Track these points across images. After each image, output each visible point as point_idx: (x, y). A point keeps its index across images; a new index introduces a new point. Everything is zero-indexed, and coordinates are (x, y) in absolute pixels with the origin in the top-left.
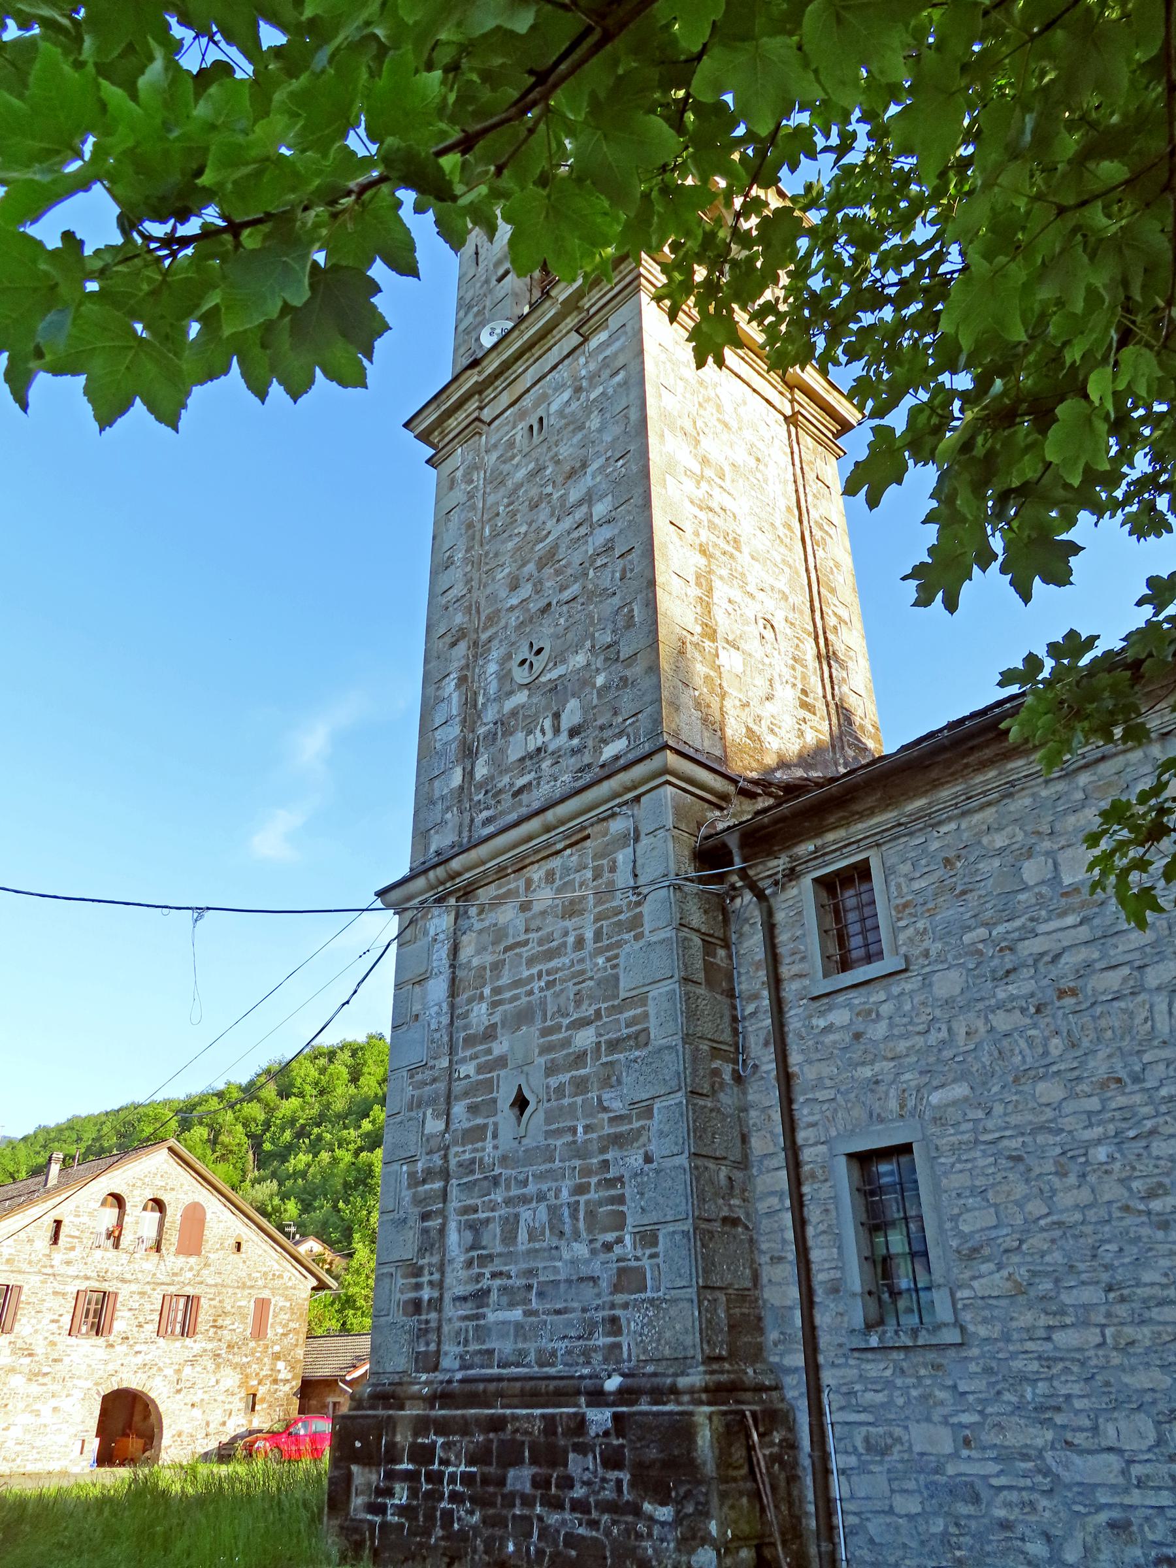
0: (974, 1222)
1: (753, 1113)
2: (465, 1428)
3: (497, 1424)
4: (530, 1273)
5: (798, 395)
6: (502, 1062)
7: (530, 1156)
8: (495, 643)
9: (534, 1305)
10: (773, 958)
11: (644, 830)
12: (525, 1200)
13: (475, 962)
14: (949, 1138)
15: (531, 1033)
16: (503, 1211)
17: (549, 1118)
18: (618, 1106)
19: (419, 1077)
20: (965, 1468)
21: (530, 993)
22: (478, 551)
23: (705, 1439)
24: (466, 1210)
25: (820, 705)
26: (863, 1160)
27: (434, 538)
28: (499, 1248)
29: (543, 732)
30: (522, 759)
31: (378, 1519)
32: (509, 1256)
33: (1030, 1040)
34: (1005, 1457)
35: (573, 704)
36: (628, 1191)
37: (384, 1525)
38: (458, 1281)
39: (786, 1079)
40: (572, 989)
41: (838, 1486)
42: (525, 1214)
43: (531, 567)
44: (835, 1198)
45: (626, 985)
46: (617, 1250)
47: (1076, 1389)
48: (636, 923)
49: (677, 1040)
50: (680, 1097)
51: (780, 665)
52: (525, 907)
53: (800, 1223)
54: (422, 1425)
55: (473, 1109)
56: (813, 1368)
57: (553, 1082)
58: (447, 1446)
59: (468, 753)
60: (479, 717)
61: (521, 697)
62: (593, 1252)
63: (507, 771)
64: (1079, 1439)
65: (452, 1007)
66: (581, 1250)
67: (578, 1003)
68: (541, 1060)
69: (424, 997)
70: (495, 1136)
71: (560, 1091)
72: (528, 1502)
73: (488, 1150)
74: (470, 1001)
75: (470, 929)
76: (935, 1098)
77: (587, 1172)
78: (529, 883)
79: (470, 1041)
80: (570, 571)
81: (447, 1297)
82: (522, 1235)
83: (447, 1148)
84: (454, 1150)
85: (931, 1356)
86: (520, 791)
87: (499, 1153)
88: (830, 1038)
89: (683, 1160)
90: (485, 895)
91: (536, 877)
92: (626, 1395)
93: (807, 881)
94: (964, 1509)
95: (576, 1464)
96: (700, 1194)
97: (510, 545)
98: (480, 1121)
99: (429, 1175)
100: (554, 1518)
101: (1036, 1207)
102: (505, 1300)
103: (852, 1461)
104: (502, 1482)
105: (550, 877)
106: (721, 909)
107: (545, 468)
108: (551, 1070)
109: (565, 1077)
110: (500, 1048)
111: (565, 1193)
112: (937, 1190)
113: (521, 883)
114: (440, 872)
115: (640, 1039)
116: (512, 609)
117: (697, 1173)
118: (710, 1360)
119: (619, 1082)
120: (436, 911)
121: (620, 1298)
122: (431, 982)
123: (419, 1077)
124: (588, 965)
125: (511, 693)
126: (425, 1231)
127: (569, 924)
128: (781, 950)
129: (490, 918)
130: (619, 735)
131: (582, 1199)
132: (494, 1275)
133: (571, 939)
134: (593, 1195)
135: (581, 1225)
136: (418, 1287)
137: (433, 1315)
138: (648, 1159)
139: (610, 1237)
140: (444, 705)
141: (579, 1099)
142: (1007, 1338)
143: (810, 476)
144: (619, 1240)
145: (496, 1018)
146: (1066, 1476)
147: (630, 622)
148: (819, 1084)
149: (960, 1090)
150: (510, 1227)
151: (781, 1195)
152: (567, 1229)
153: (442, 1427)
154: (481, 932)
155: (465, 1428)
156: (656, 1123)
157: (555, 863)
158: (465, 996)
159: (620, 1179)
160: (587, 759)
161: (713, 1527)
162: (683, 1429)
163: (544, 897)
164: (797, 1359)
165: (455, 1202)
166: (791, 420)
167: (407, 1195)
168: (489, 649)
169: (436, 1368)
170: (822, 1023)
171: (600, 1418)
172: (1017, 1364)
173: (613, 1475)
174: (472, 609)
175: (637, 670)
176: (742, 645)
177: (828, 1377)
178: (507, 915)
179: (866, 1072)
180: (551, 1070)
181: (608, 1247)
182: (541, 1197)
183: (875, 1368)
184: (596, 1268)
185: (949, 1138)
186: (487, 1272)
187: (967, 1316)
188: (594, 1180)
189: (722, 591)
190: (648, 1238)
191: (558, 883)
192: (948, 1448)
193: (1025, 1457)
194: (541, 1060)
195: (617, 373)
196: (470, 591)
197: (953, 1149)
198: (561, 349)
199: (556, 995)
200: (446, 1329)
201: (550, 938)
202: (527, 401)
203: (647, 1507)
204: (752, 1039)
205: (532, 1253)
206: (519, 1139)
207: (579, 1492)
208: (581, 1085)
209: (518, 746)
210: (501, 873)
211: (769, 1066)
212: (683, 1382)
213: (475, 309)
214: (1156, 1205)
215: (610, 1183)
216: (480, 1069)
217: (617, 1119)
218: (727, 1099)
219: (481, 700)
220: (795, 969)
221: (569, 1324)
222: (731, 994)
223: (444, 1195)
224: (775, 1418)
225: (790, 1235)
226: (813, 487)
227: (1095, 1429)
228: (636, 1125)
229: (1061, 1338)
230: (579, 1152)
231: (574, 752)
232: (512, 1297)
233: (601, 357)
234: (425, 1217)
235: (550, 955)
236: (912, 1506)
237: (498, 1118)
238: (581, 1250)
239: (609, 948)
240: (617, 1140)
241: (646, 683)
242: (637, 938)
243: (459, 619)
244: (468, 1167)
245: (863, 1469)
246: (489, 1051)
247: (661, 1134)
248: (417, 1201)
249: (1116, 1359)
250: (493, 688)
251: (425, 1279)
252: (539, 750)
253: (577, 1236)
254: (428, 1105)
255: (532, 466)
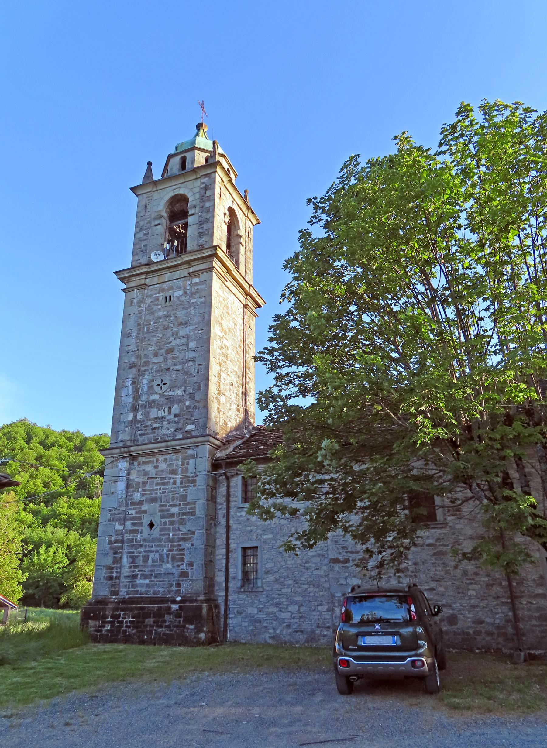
0: (269, 565)
1: (218, 534)
2: (131, 610)
3: (142, 609)
4: (152, 571)
5: (248, 298)
6: (145, 512)
7: (154, 540)
8: (147, 373)
9: (153, 579)
10: (228, 495)
11: (199, 456)
12: (151, 551)
13: (136, 480)
14: (266, 546)
15: (157, 505)
16: (144, 554)
17: (161, 530)
18: (184, 530)
19: (113, 512)
20: (258, 616)
21: (157, 493)
22: (141, 336)
23: (205, 611)
24: (130, 553)
25: (241, 409)
26: (244, 549)
27: (123, 322)
28: (141, 563)
29: (164, 411)
30: (156, 418)
31: (99, 634)
32: (145, 566)
33: (288, 527)
34: (268, 614)
35: (176, 406)
36: (185, 553)
37: (101, 635)
38: (126, 571)
39: (228, 527)
40: (171, 495)
41: (229, 621)
42: (151, 555)
43: (163, 351)
44: (237, 557)
45: (189, 499)
46: (181, 567)
47: (284, 600)
48: (194, 481)
49: (204, 516)
50: (204, 531)
51: (233, 397)
52: (156, 467)
53: (227, 562)
54: (116, 609)
55: (134, 524)
56: (226, 596)
57: (163, 520)
58: (124, 614)
59: (135, 409)
60: (139, 397)
61: (156, 397)
62: (173, 567)
63: (150, 420)
64: (283, 610)
65: (127, 492)
66: (169, 566)
67: (173, 500)
68: (160, 514)
69: (116, 487)
70: (141, 533)
71: (165, 523)
72: (152, 626)
73: (139, 536)
74: (134, 491)
75: (135, 469)
76: (265, 537)
77: (174, 546)
78: (157, 460)
79: (133, 504)
80: (178, 360)
81: (122, 576)
82: (150, 561)
83: (123, 534)
84: (126, 535)
85: (255, 593)
86: (155, 428)
87: (142, 538)
88: (241, 518)
89: (203, 546)
90: (141, 459)
91: (160, 459)
92: (181, 602)
93: (240, 477)
94: (257, 624)
95: (167, 617)
96: (206, 555)
97: (155, 339)
98: (136, 528)
99: (116, 541)
100: (160, 630)
101: (283, 563)
102: (143, 578)
103: (233, 616)
104: (144, 622)
105: (165, 460)
106: (215, 480)
107: (171, 316)
108: (162, 517)
109: (167, 520)
110: (145, 507)
111: (165, 551)
112: (262, 557)
113: (155, 460)
114: (126, 449)
115: (193, 514)
116: (154, 363)
117: (206, 550)
118: (205, 594)
119: (185, 524)
120: (122, 460)
121: (181, 579)
122: (119, 483)
123: (113, 512)
124: (177, 490)
125: (152, 394)
126: (115, 557)
127: (171, 476)
128: (231, 493)
129: (143, 467)
130: (193, 423)
131: (171, 553)
132: (139, 571)
133: (172, 481)
134: (174, 552)
135: (170, 559)
136: (112, 573)
137: (117, 581)
138: (192, 545)
139: (179, 563)
140: (126, 389)
141: (171, 527)
142: (272, 590)
143: (248, 326)
144: (182, 565)
145: (143, 499)
146: (280, 617)
147: (199, 388)
148: (237, 529)
149: (270, 536)
150: (146, 559)
151: (223, 555)
152: (165, 560)
153: (123, 610)
154: (138, 471)
155: (131, 610)
156: (196, 536)
157: (168, 457)
158: (132, 490)
159: (184, 549)
160: (180, 426)
161: (205, 629)
162: (200, 608)
163: (163, 466)
164: (223, 594)
165: (126, 550)
166: (245, 306)
167: (108, 547)
168: (144, 374)
169: (118, 595)
170: (239, 514)
171: (175, 607)
172: (273, 595)
173: (178, 619)
174: (139, 357)
175: (201, 405)
176: (226, 393)
177: (230, 598)
178: (149, 468)
179: (249, 528)
180: (162, 517)
181: (178, 566)
182: (157, 551)
183: (243, 596)
184: (174, 571)
185: (266, 546)
186: (137, 570)
187: (264, 585)
188: (175, 549)
189: (223, 375)
190: (191, 565)
191: (168, 463)
192: (256, 612)
193: (272, 614)
194: (160, 514)
195: (202, 297)
196: (138, 350)
197: (267, 549)
198: (180, 273)
199: (165, 496)
200: (121, 584)
201: (164, 479)
202: (165, 286)
203: (187, 626)
204: (220, 515)
205: (152, 566)
206: (150, 535)
207: (167, 624)
208: (172, 523)
209: (154, 413)
210: (148, 454)
211: (224, 523)
212: (199, 598)
213: (144, 232)
214: (307, 565)
215: (181, 550)
216: (136, 513)
217: (185, 534)
218: (212, 530)
219: (140, 392)
220: (234, 499)
221: (164, 584)
222: (215, 502)
223: (122, 548)
224: (217, 607)
225: (224, 565)
226: (249, 330)
227: (287, 608)
228: (189, 536)
229: (284, 590)
230: (171, 541)
231: (175, 422)
232: (145, 577)
233: (196, 288)
234: (115, 553)
235: (164, 484)
236: (246, 624)
237: (143, 528)
238: (169, 566)
239: (185, 487)
240: (184, 539)
241: (203, 410)
242: (194, 486)
243: (133, 359)
244: (132, 541)
245: (235, 617)
246: (140, 508)
247: (197, 539)
248: (111, 548)
249: (293, 594)
250: (146, 389)
251: (115, 571)
252: (163, 417)
253: (168, 562)
254: (116, 521)
255: (165, 313)
